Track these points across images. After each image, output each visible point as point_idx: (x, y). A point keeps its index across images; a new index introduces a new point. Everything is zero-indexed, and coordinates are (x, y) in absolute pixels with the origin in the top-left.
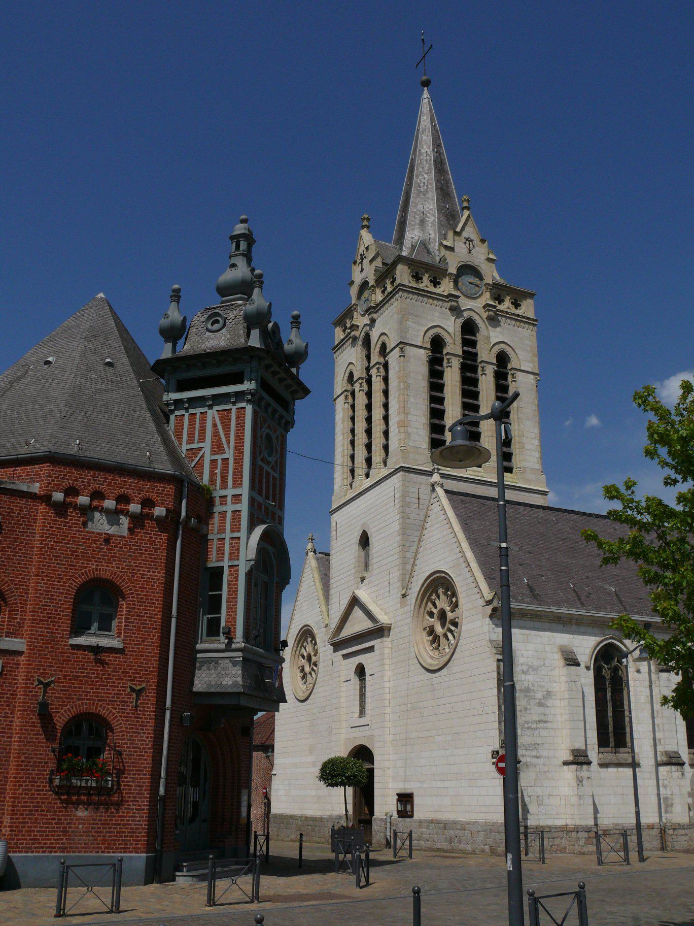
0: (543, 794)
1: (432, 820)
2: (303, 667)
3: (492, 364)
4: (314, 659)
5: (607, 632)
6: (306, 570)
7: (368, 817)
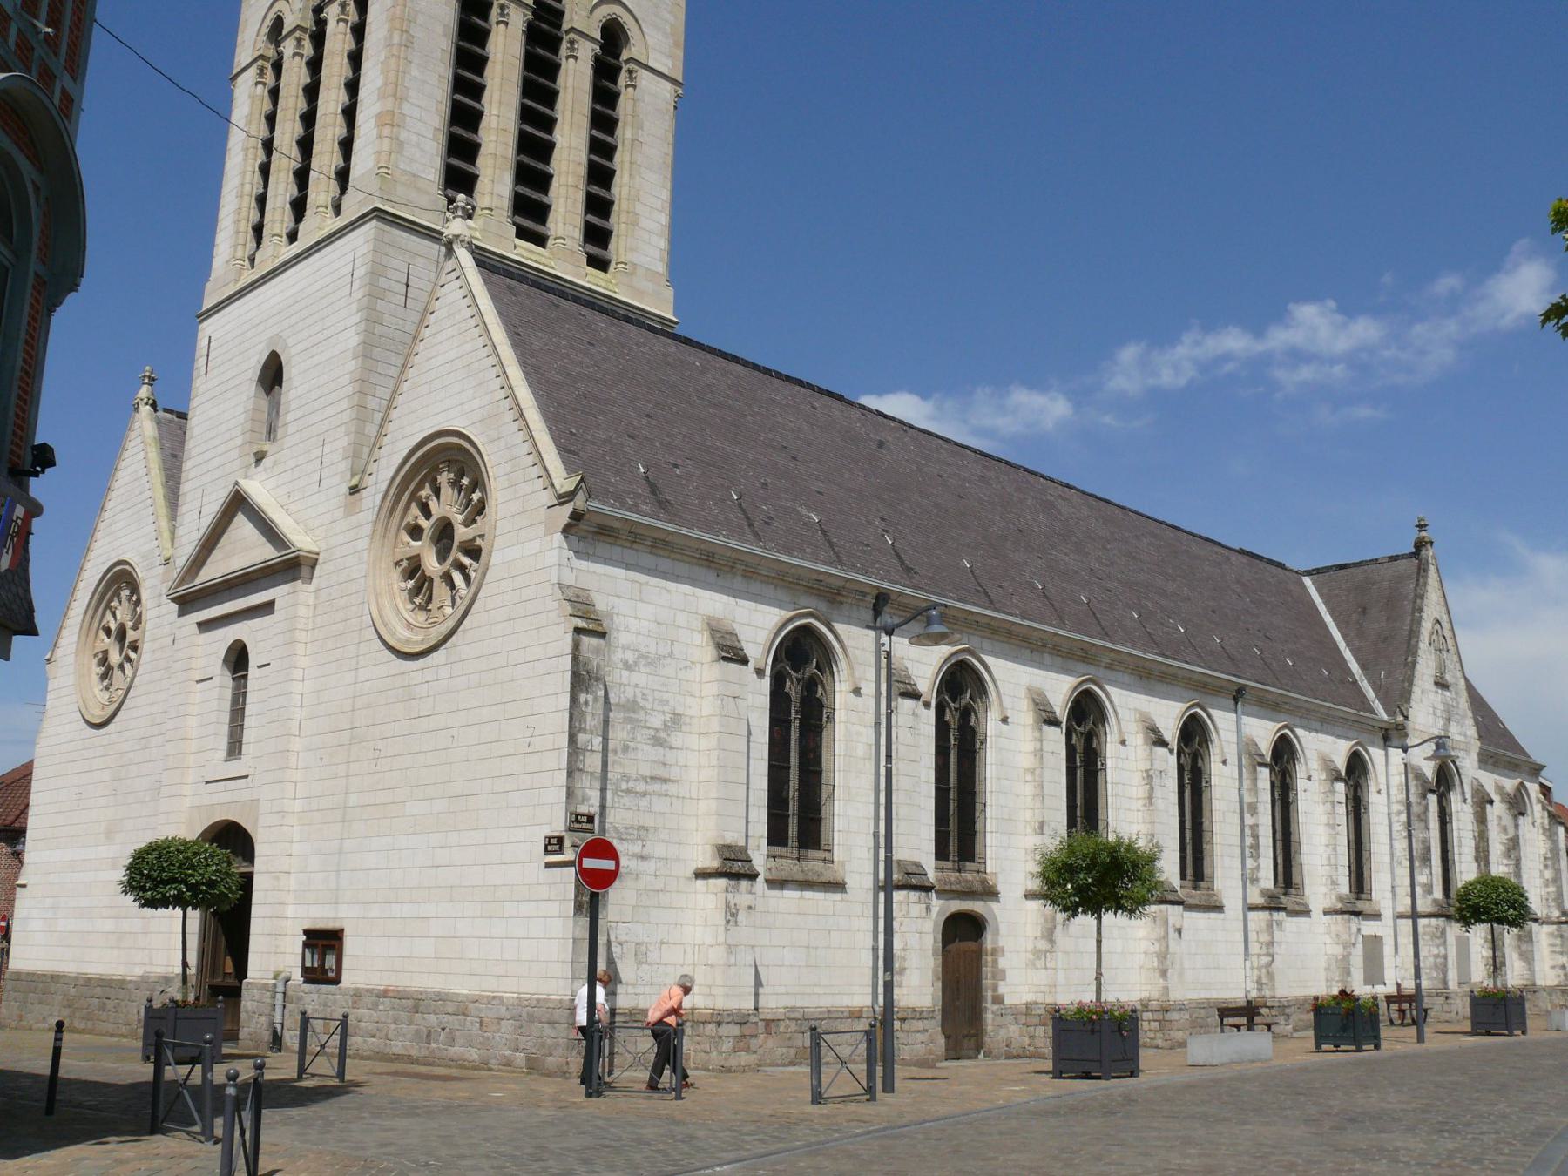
0: (647, 940)
1: (386, 991)
2: (105, 653)
3: (592, 39)
4: (131, 635)
5: (804, 600)
6: (130, 445)
7: (231, 981)
